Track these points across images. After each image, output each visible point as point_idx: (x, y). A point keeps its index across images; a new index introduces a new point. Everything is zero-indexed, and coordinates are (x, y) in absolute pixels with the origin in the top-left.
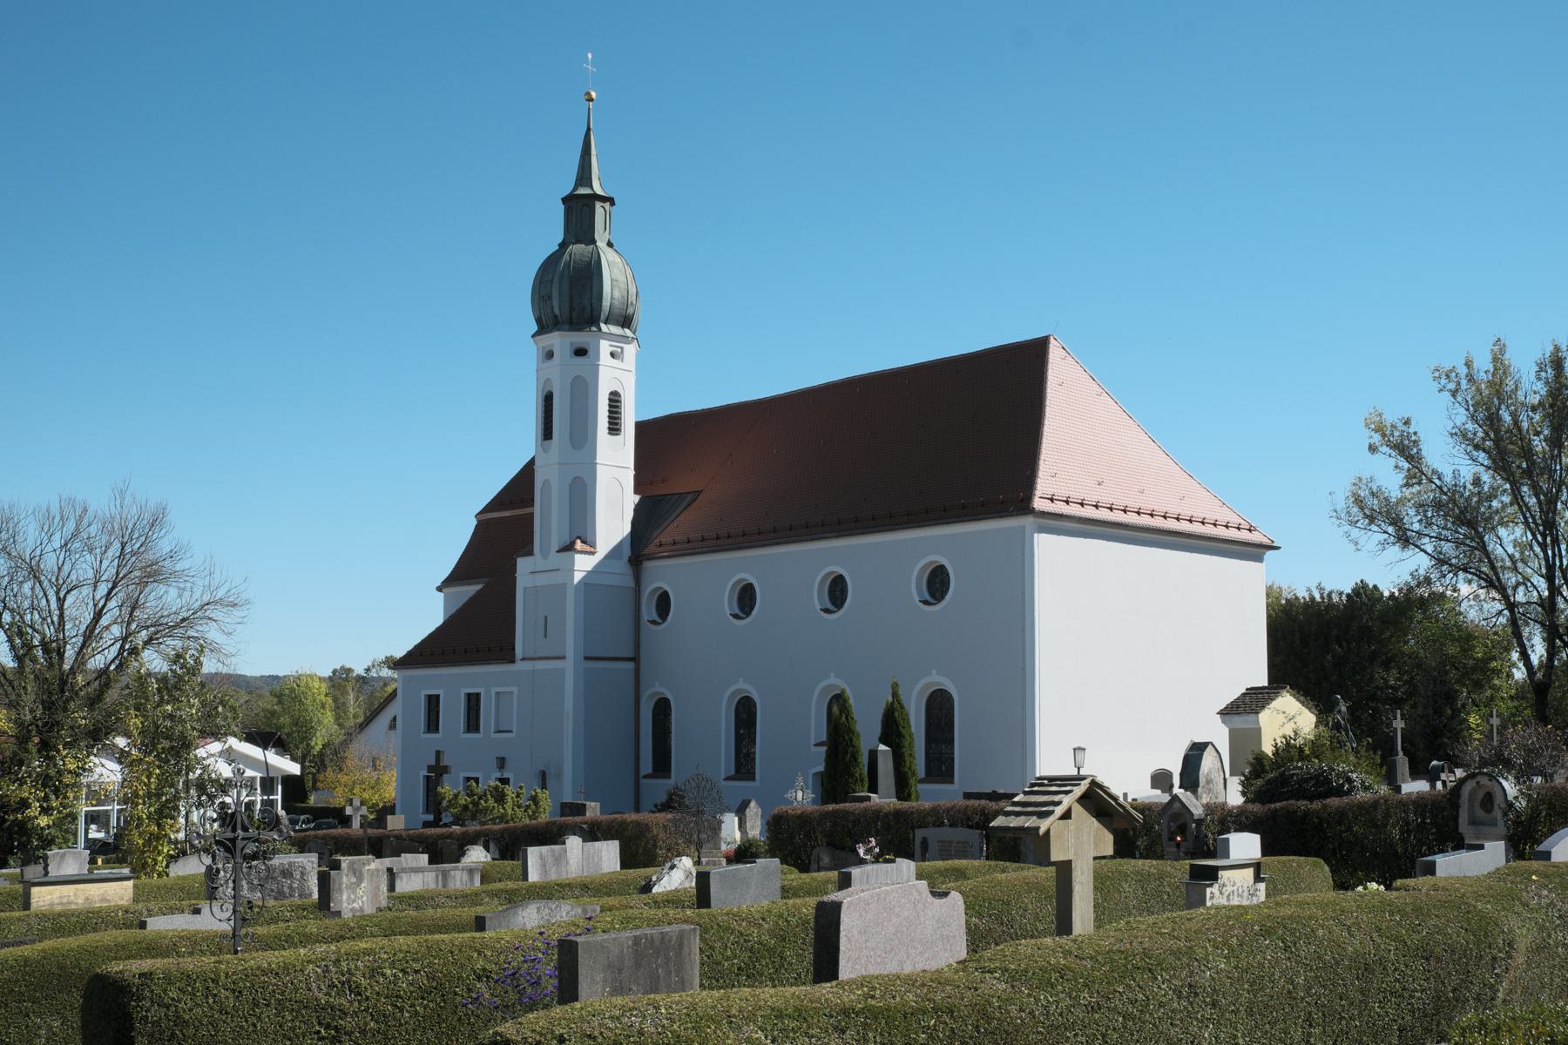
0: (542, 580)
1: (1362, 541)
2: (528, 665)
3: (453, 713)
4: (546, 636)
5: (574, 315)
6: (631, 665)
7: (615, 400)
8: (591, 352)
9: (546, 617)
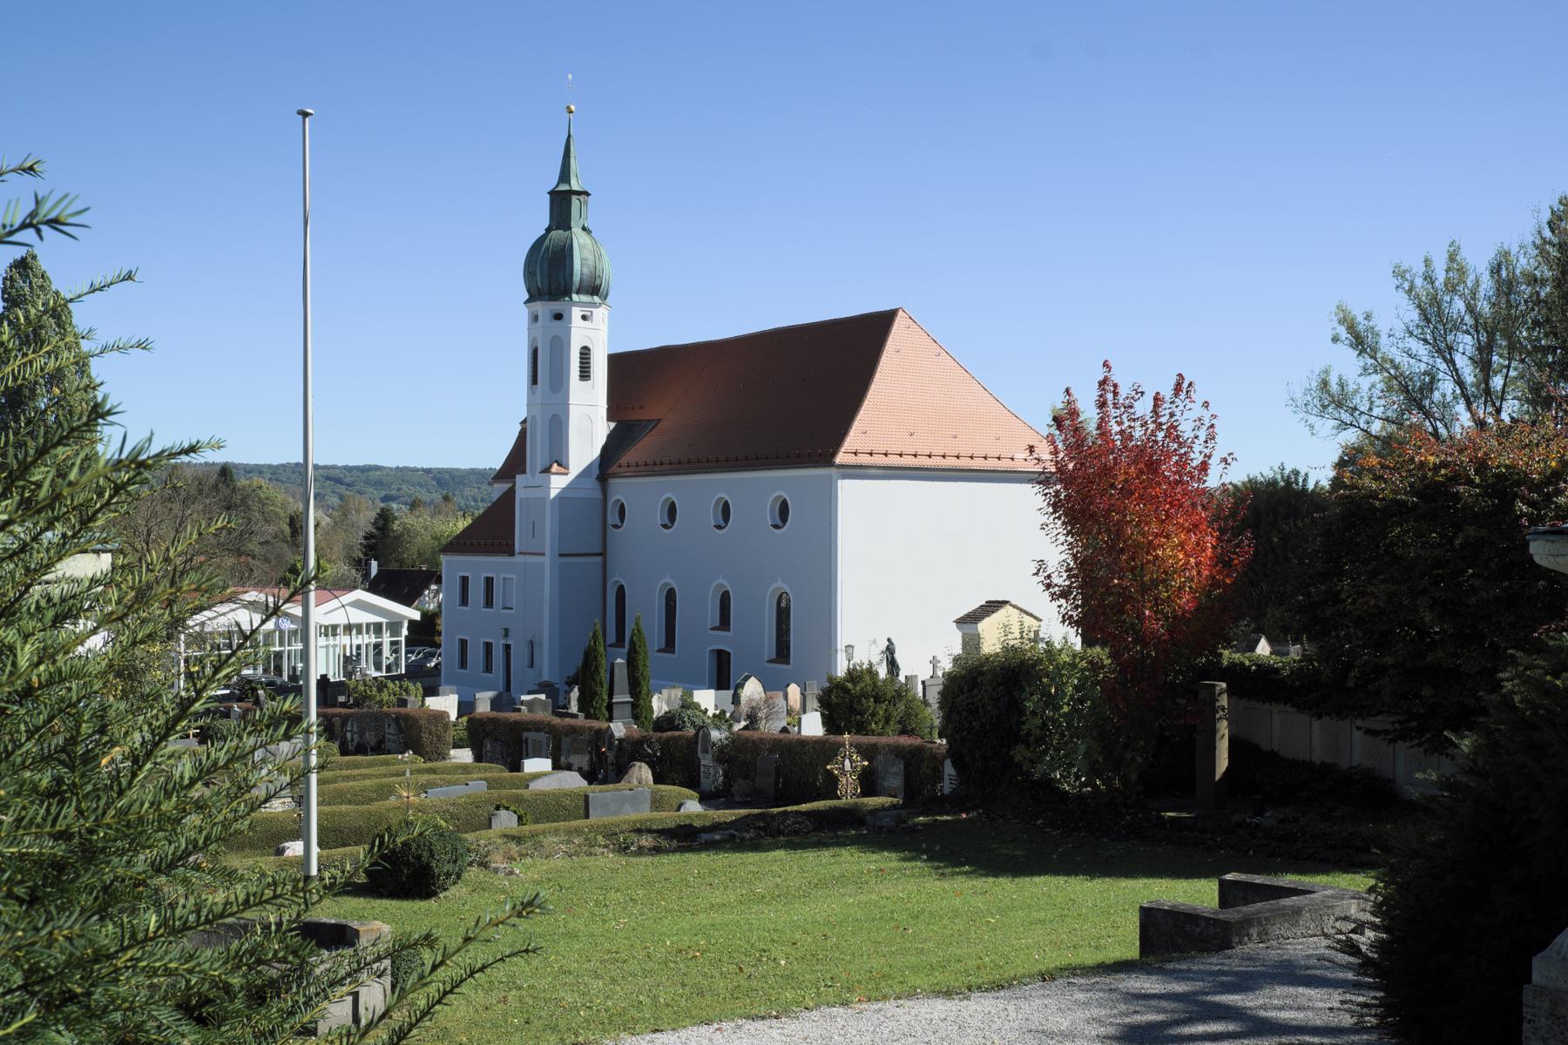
0: (532, 493)
1: (1317, 427)
3: (477, 592)
5: (553, 287)
6: (599, 559)
7: (585, 353)
8: (565, 316)
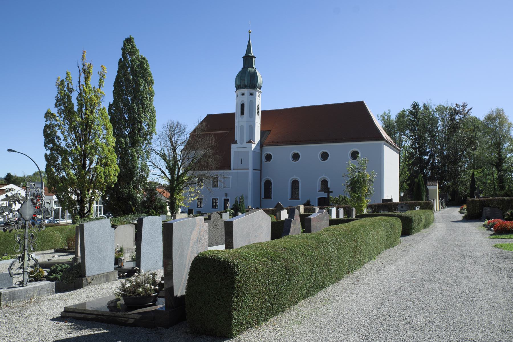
2: (236, 171)
4: (241, 163)
6: (259, 172)
8: (254, 95)
9: (242, 159)
